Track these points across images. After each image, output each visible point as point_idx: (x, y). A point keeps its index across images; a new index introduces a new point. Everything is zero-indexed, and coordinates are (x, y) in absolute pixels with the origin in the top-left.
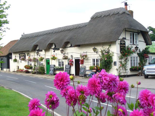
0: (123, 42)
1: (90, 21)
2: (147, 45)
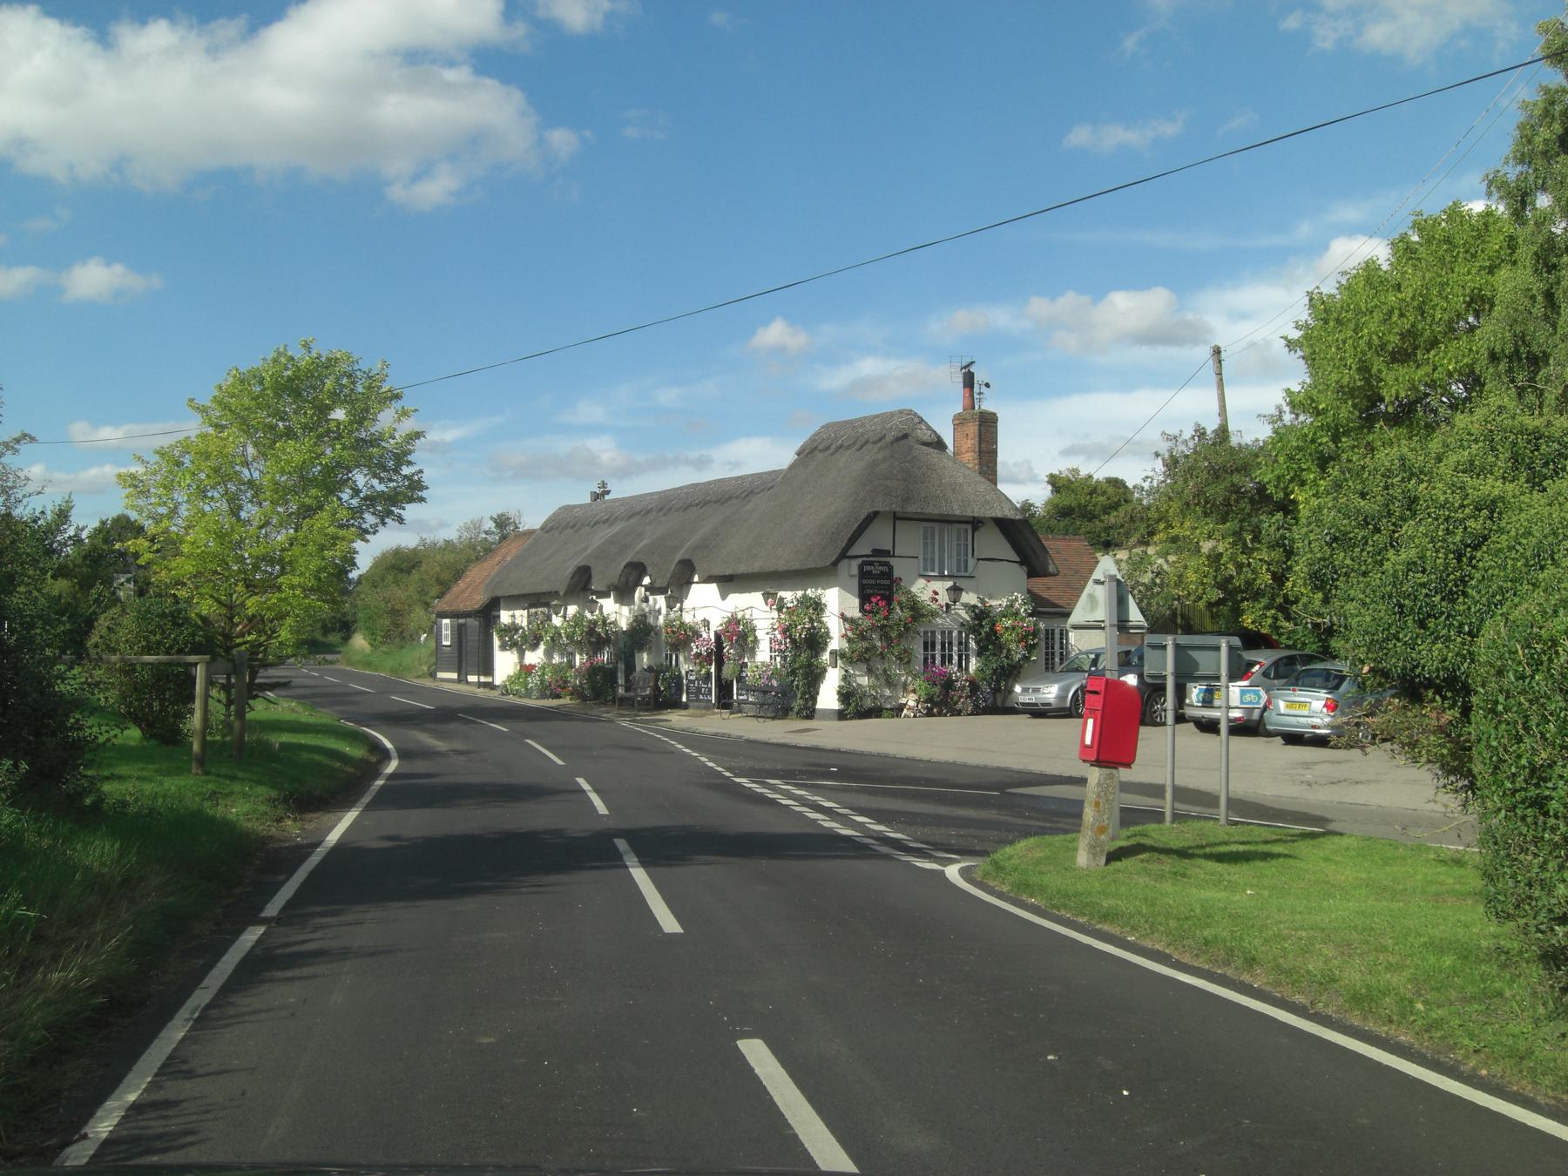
0: (877, 570)
1: (793, 466)
2: (1030, 575)
